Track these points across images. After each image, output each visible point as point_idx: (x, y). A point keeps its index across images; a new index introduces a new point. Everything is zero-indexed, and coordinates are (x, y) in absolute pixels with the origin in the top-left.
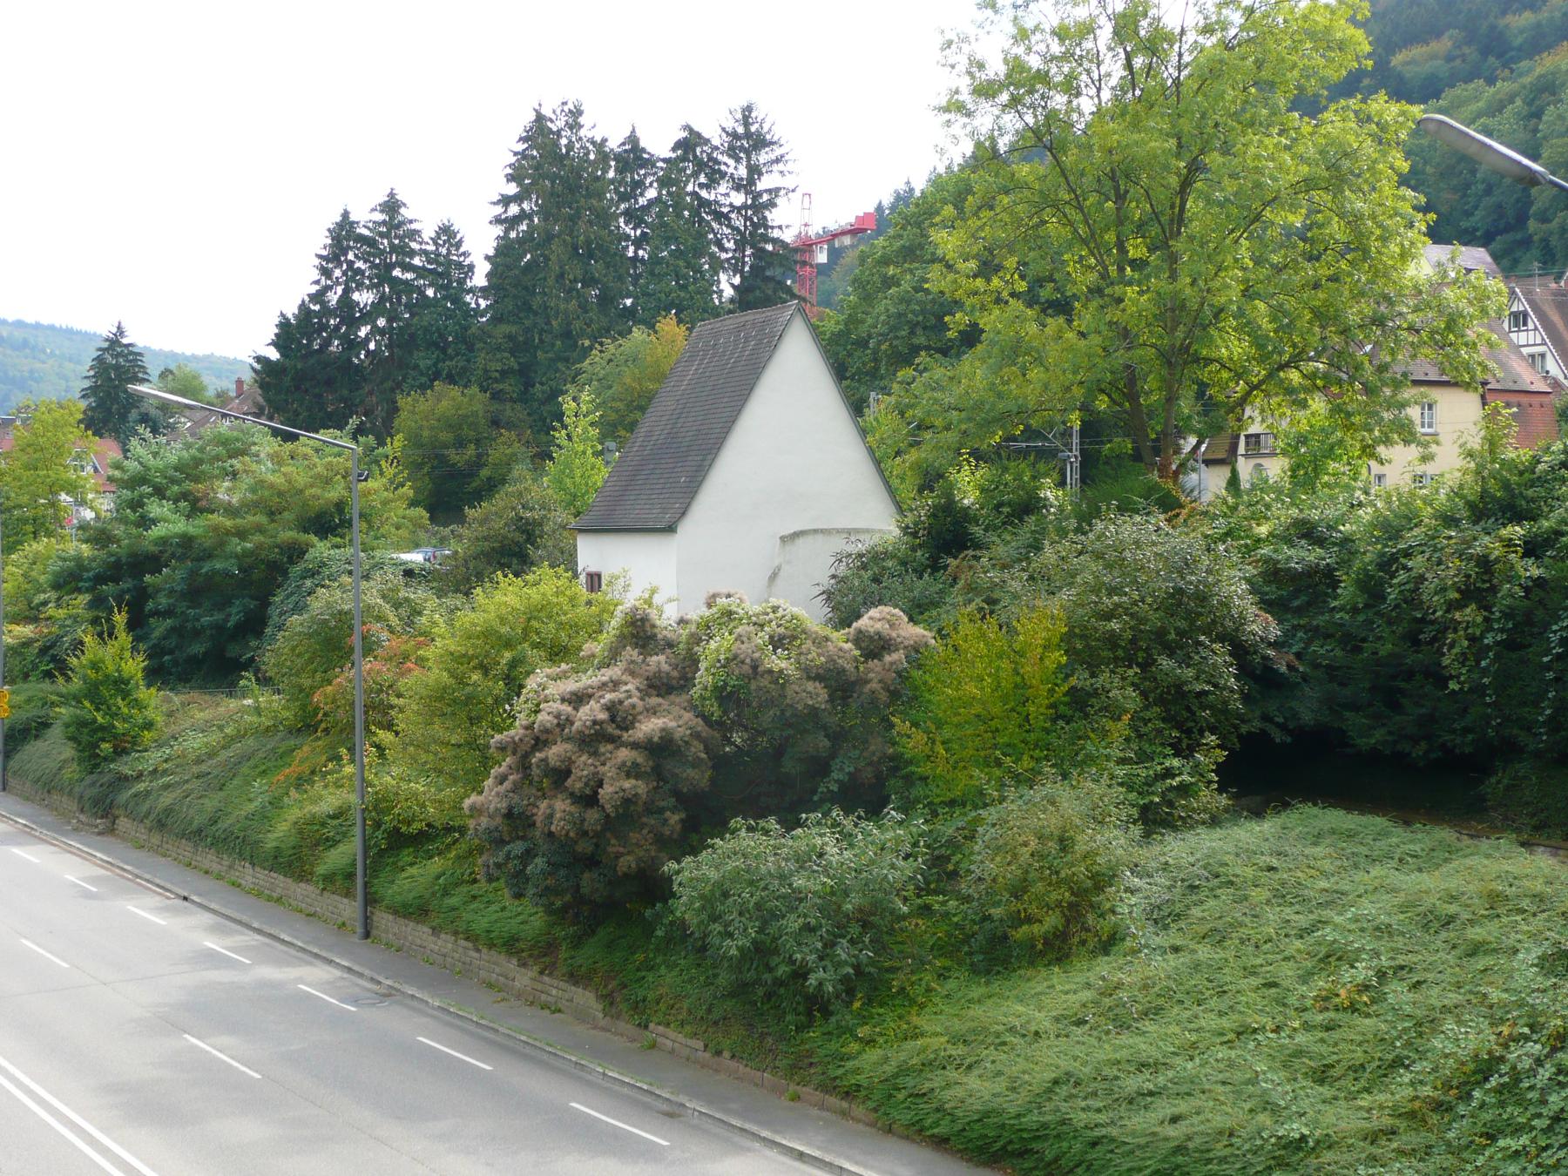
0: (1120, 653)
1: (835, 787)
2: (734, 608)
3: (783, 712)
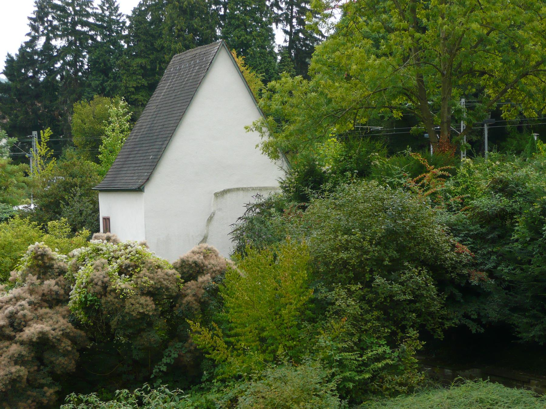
0: (351, 274)
1: (164, 369)
2: (100, 247)
3: (124, 317)
